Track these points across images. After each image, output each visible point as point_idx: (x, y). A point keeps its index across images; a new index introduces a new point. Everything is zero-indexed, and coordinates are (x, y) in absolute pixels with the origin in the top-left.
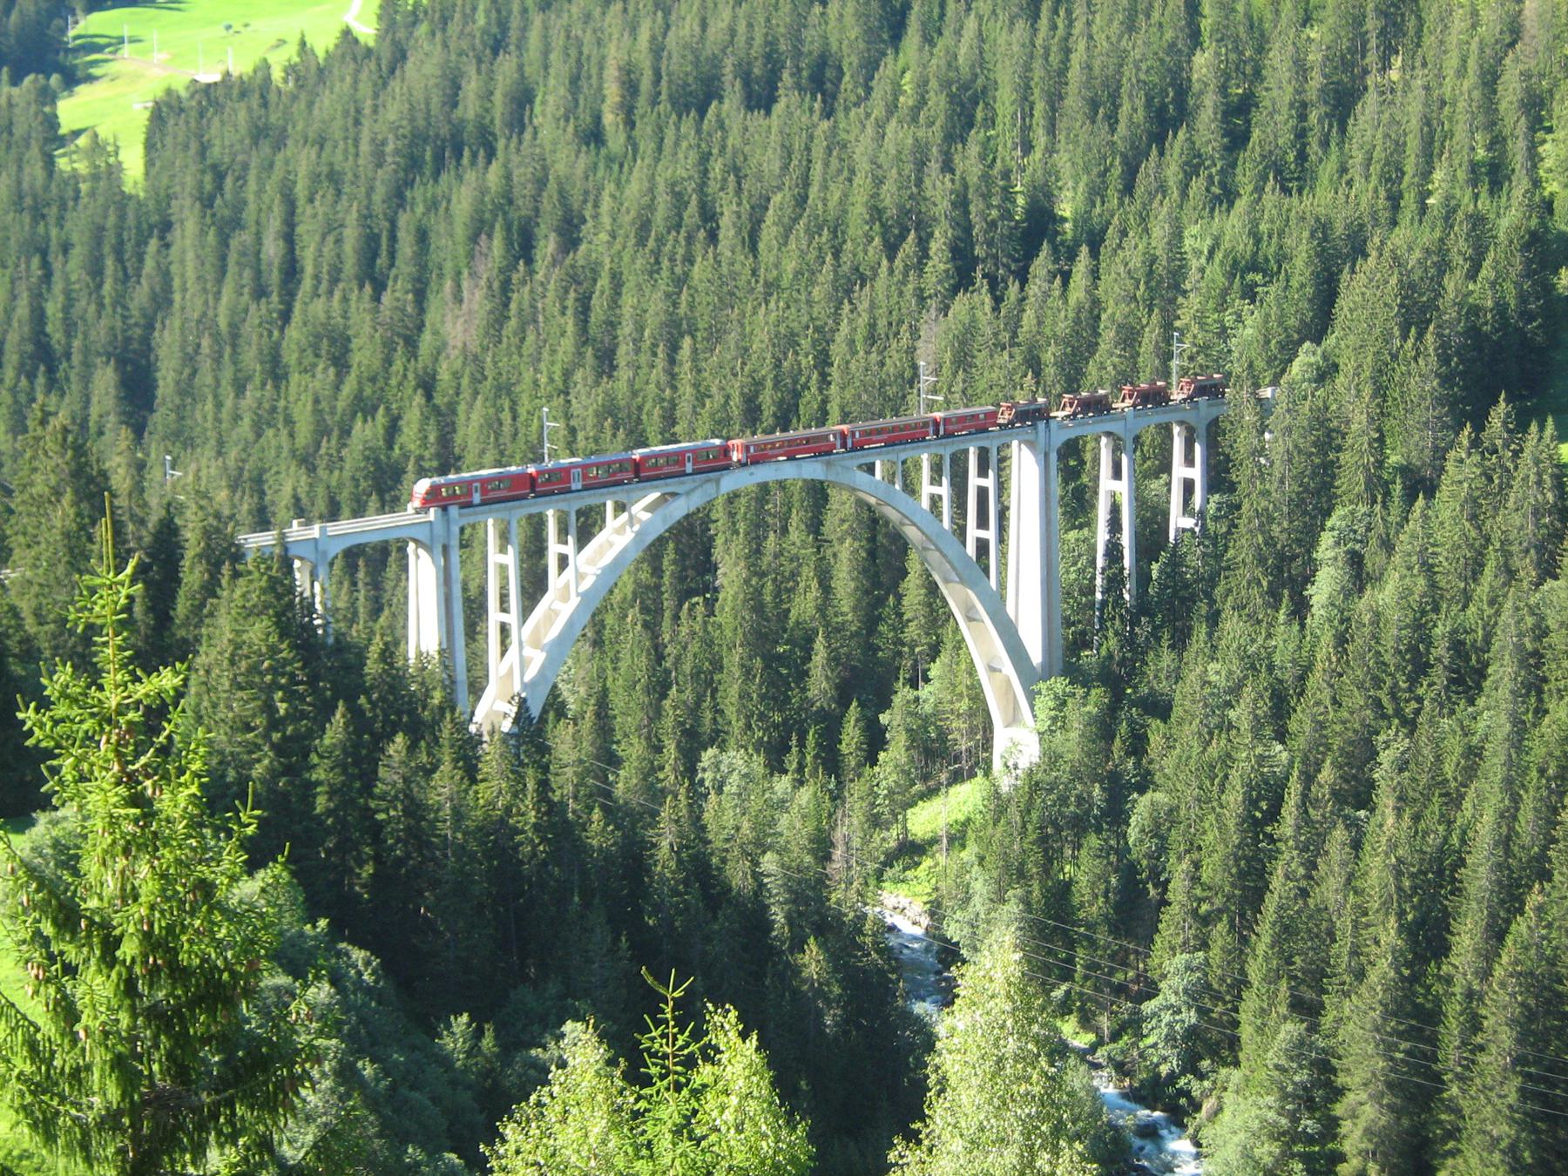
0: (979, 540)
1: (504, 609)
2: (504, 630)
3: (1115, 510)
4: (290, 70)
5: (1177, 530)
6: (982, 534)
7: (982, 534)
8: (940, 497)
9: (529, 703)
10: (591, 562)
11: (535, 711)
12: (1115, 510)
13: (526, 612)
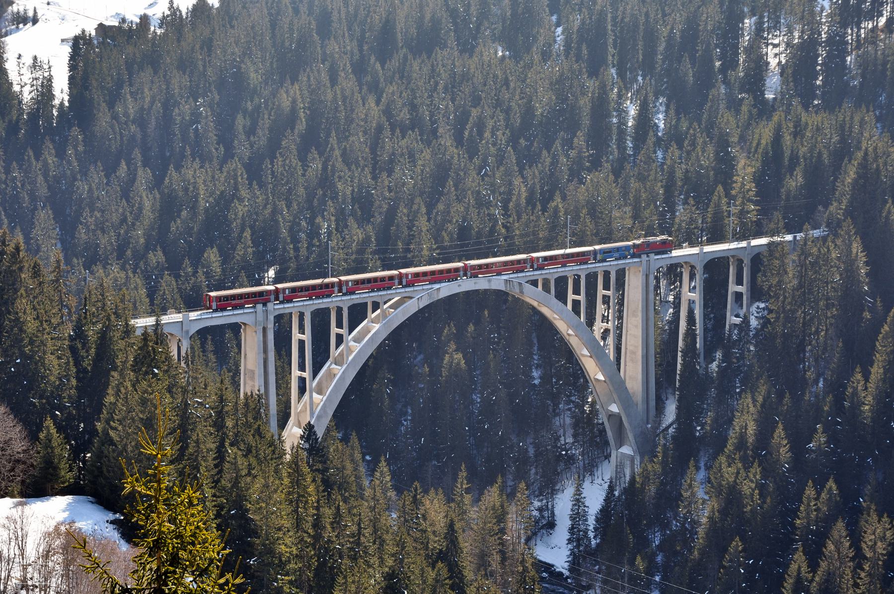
0: (574, 301)
1: (302, 368)
2: (302, 380)
3: (691, 313)
4: (163, 21)
5: (730, 326)
6: (577, 297)
7: (577, 297)
8: (579, 301)
9: (316, 429)
10: (357, 340)
11: (320, 432)
12: (691, 313)
13: (315, 374)
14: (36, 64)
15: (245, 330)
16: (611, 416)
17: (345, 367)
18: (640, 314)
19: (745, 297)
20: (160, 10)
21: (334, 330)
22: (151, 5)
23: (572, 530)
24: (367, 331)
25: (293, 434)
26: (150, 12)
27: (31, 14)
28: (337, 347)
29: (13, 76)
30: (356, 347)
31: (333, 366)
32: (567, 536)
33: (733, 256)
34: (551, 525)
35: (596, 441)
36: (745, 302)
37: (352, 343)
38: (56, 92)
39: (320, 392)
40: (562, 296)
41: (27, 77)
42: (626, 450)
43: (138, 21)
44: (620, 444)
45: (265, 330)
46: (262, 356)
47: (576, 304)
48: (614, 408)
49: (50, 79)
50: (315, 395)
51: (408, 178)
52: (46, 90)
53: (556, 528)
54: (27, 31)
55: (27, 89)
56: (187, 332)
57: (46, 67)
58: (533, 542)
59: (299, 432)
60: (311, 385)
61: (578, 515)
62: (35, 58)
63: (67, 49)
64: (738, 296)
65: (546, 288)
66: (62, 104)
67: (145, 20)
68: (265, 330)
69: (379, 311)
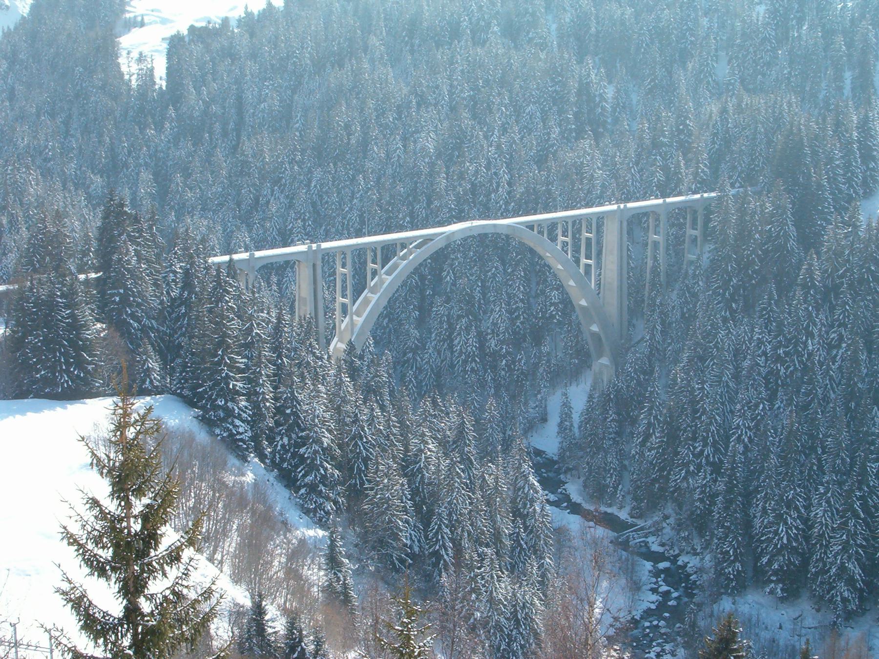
14: (141, 59)
15: (299, 267)
16: (593, 334)
17: (379, 294)
18: (615, 252)
19: (699, 239)
20: (240, 13)
21: (371, 265)
22: (232, 9)
23: (560, 425)
24: (395, 266)
25: (337, 346)
26: (230, 15)
27: (139, 19)
28: (372, 279)
29: (124, 69)
30: (389, 279)
31: (369, 295)
32: (556, 429)
33: (690, 207)
34: (544, 420)
35: (582, 358)
36: (699, 243)
37: (384, 276)
38: (157, 81)
39: (359, 315)
40: (553, 239)
41: (134, 68)
42: (605, 361)
43: (220, 22)
44: (600, 356)
45: (314, 265)
46: (312, 287)
47: (565, 244)
48: (595, 328)
49: (152, 70)
50: (355, 318)
51: (429, 142)
52: (148, 76)
53: (548, 423)
54: (136, 32)
55: (134, 78)
56: (253, 267)
57: (149, 60)
58: (529, 434)
59: (342, 346)
60: (352, 309)
61: (566, 416)
62: (141, 54)
63: (165, 45)
64: (694, 240)
65: (541, 232)
66: (161, 88)
67: (225, 21)
68: (314, 265)
69: (405, 250)
